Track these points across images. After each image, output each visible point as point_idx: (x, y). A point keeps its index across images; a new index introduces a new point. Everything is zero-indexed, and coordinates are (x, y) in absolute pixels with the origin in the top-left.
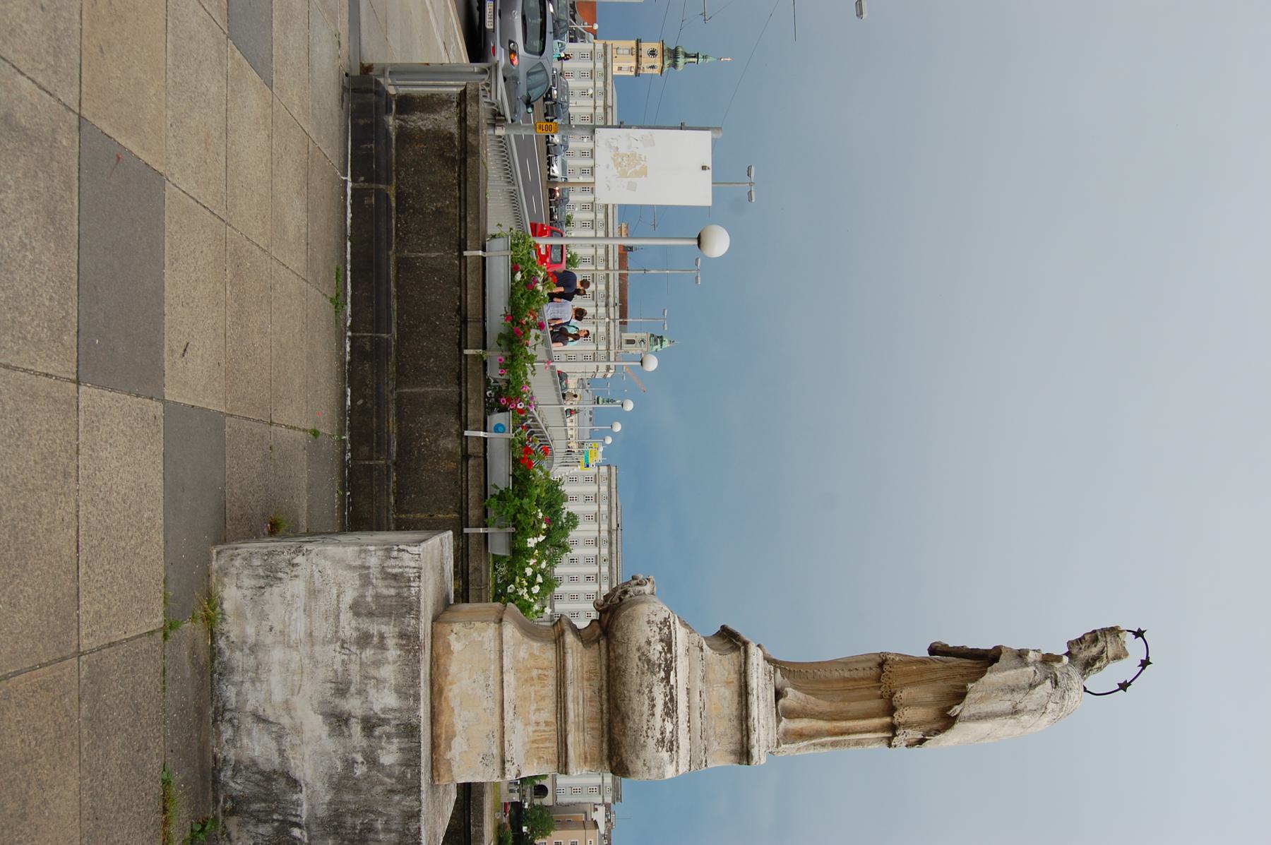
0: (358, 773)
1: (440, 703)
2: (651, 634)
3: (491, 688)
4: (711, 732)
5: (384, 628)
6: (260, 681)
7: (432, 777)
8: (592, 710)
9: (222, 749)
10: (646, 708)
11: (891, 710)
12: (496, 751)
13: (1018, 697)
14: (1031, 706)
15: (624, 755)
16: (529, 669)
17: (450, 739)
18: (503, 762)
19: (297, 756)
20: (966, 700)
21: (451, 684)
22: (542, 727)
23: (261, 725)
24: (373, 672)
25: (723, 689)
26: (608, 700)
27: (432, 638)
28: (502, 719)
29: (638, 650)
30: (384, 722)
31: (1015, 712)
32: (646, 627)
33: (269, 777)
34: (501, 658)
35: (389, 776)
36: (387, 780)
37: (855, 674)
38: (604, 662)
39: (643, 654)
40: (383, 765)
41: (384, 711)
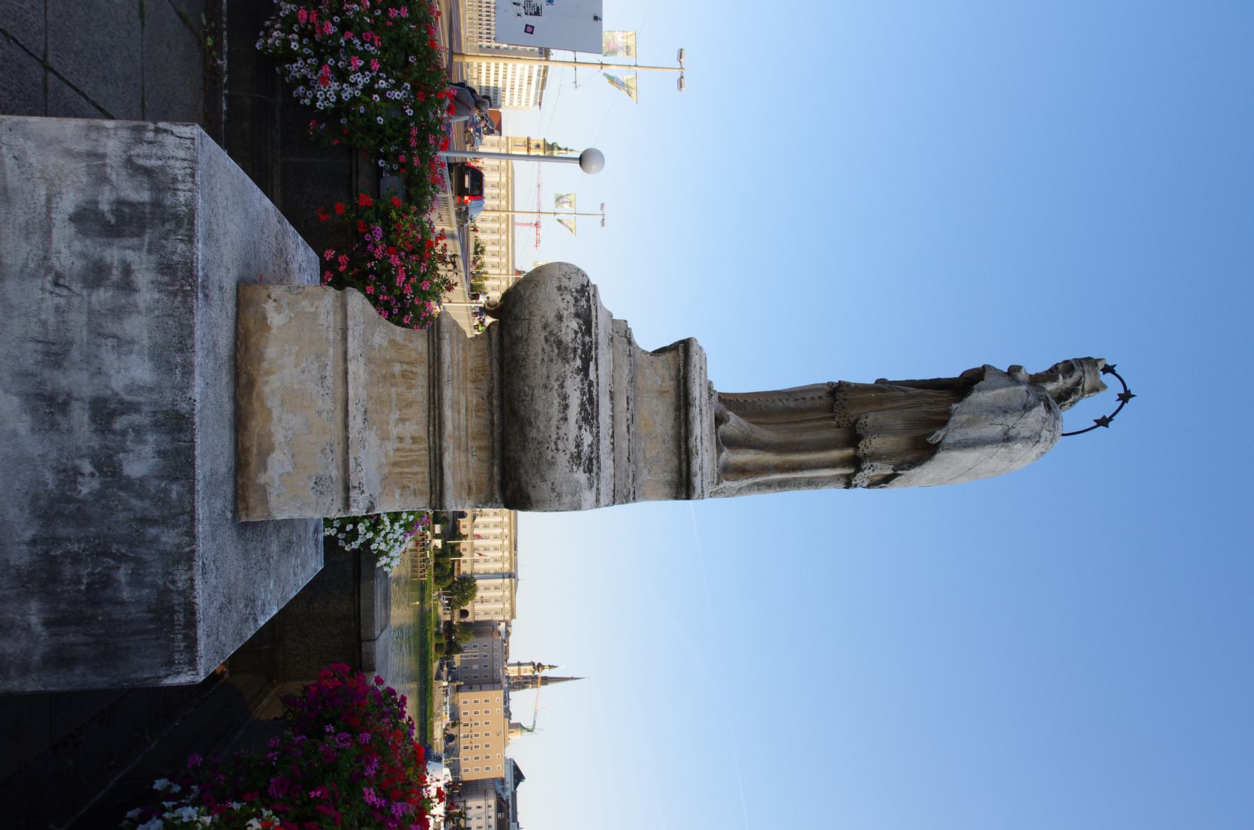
0: (85, 490)
2: (563, 305)
3: (329, 381)
4: (640, 456)
5: (131, 256)
7: (235, 512)
8: (476, 423)
10: (555, 410)
12: (335, 473)
13: (1011, 420)
14: (1026, 433)
15: (524, 478)
16: (389, 363)
18: (347, 489)
20: (951, 424)
21: (268, 373)
22: (408, 444)
24: (111, 327)
25: (655, 401)
26: (502, 407)
27: (238, 305)
28: (346, 426)
29: (545, 327)
30: (132, 408)
32: (555, 294)
34: (345, 339)
35: (141, 497)
36: (136, 503)
38: (495, 354)
39: (551, 333)
40: (128, 478)
41: (130, 389)
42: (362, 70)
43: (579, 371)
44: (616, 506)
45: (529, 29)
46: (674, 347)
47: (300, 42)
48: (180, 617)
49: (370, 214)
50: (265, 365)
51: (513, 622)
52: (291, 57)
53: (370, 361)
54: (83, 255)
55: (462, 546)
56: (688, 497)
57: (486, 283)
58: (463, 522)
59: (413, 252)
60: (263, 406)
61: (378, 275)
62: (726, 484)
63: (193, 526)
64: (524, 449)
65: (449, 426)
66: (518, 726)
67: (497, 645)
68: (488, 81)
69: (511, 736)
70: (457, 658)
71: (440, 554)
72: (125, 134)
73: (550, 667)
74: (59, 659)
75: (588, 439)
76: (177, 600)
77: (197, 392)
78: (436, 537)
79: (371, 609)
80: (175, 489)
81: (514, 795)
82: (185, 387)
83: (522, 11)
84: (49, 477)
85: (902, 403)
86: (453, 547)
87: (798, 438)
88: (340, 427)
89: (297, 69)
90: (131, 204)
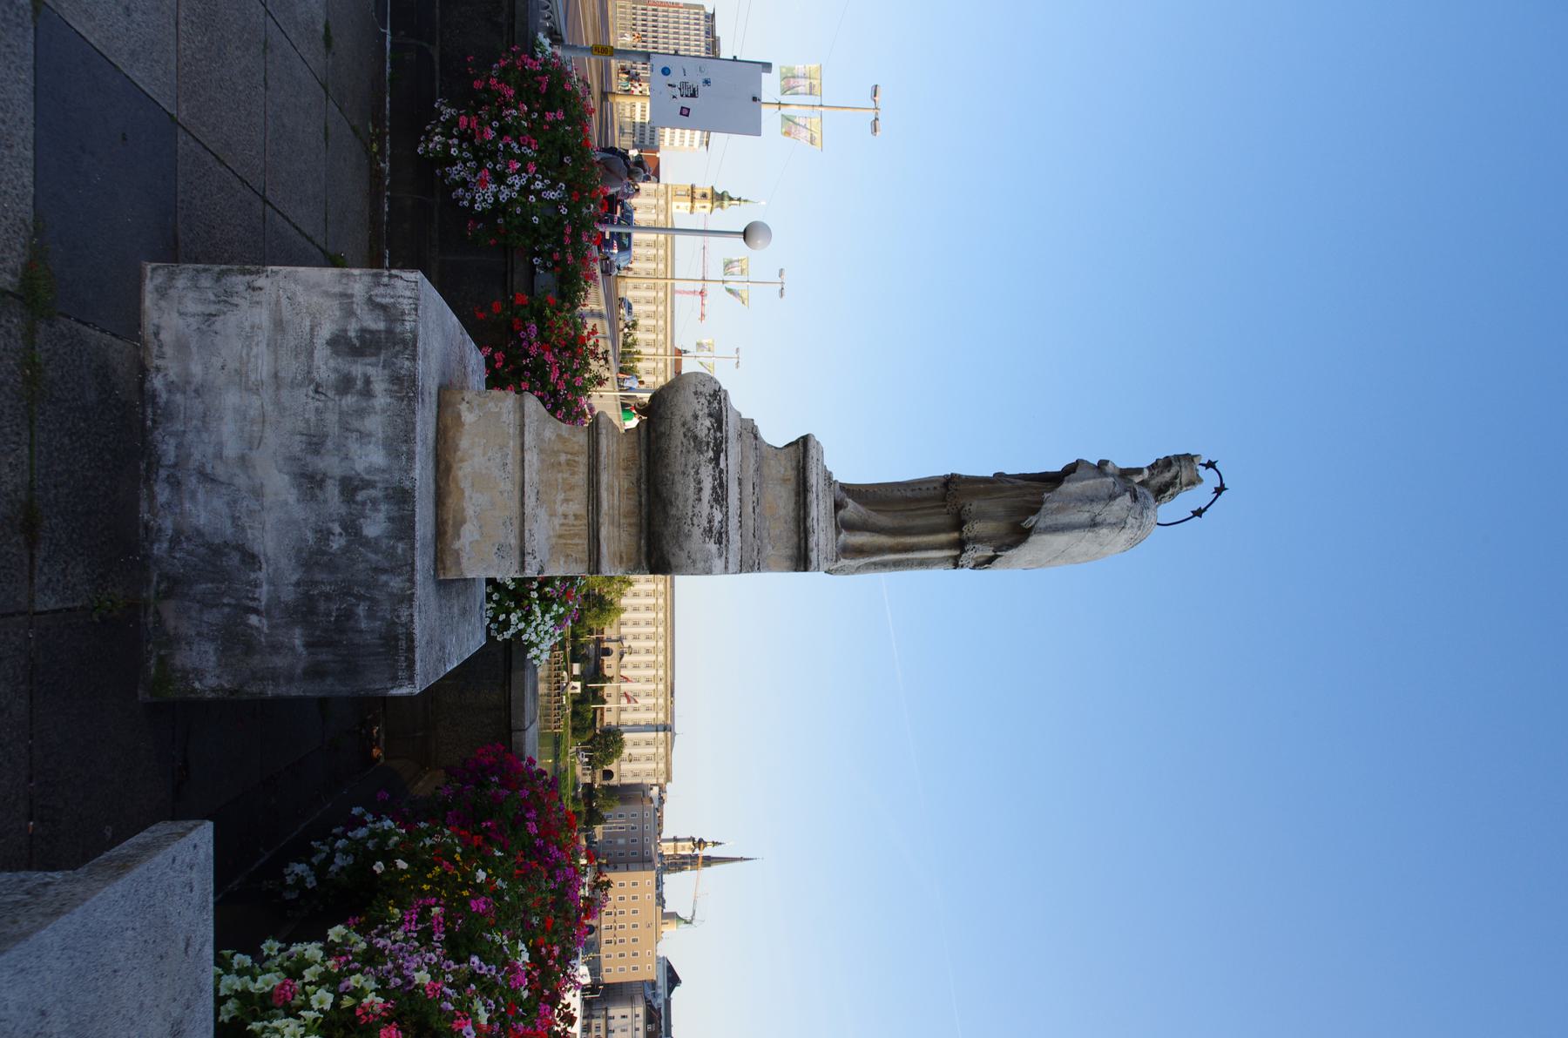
0: (335, 546)
3: (510, 467)
4: (765, 534)
5: (371, 371)
6: (207, 430)
7: (436, 570)
8: (627, 504)
9: (155, 515)
10: (691, 492)
11: (959, 525)
12: (514, 542)
13: (1097, 508)
14: (1113, 520)
17: (459, 523)
18: (523, 554)
19: (256, 525)
21: (462, 461)
22: (571, 520)
23: (209, 486)
24: (356, 424)
27: (439, 406)
28: (523, 504)
30: (369, 484)
31: (1094, 524)
32: (692, 398)
33: (217, 551)
34: (522, 434)
35: (376, 553)
36: (371, 556)
38: (644, 447)
41: (369, 470)
42: (519, 172)
43: (711, 460)
44: (743, 575)
45: (685, 112)
46: (796, 442)
47: (460, 146)
48: (403, 644)
49: (525, 312)
50: (459, 454)
51: (669, 787)
52: (452, 162)
53: (541, 451)
54: (336, 370)
55: (606, 691)
56: (806, 570)
57: (639, 365)
58: (607, 660)
59: (566, 348)
60: (458, 487)
61: (533, 372)
62: (843, 562)
63: (413, 575)
64: (666, 524)
65: (605, 506)
66: (673, 916)
67: (648, 814)
68: (643, 116)
69: (665, 929)
70: (599, 830)
71: (578, 701)
72: (367, 279)
73: (715, 844)
74: (315, 672)
75: (718, 516)
76: (401, 630)
77: (417, 473)
78: (575, 678)
79: (522, 699)
80: (400, 547)
81: (668, 1002)
82: (408, 469)
83: (678, 93)
84: (310, 536)
86: (595, 691)
87: (911, 523)
88: (518, 505)
89: (457, 172)
90: (371, 332)
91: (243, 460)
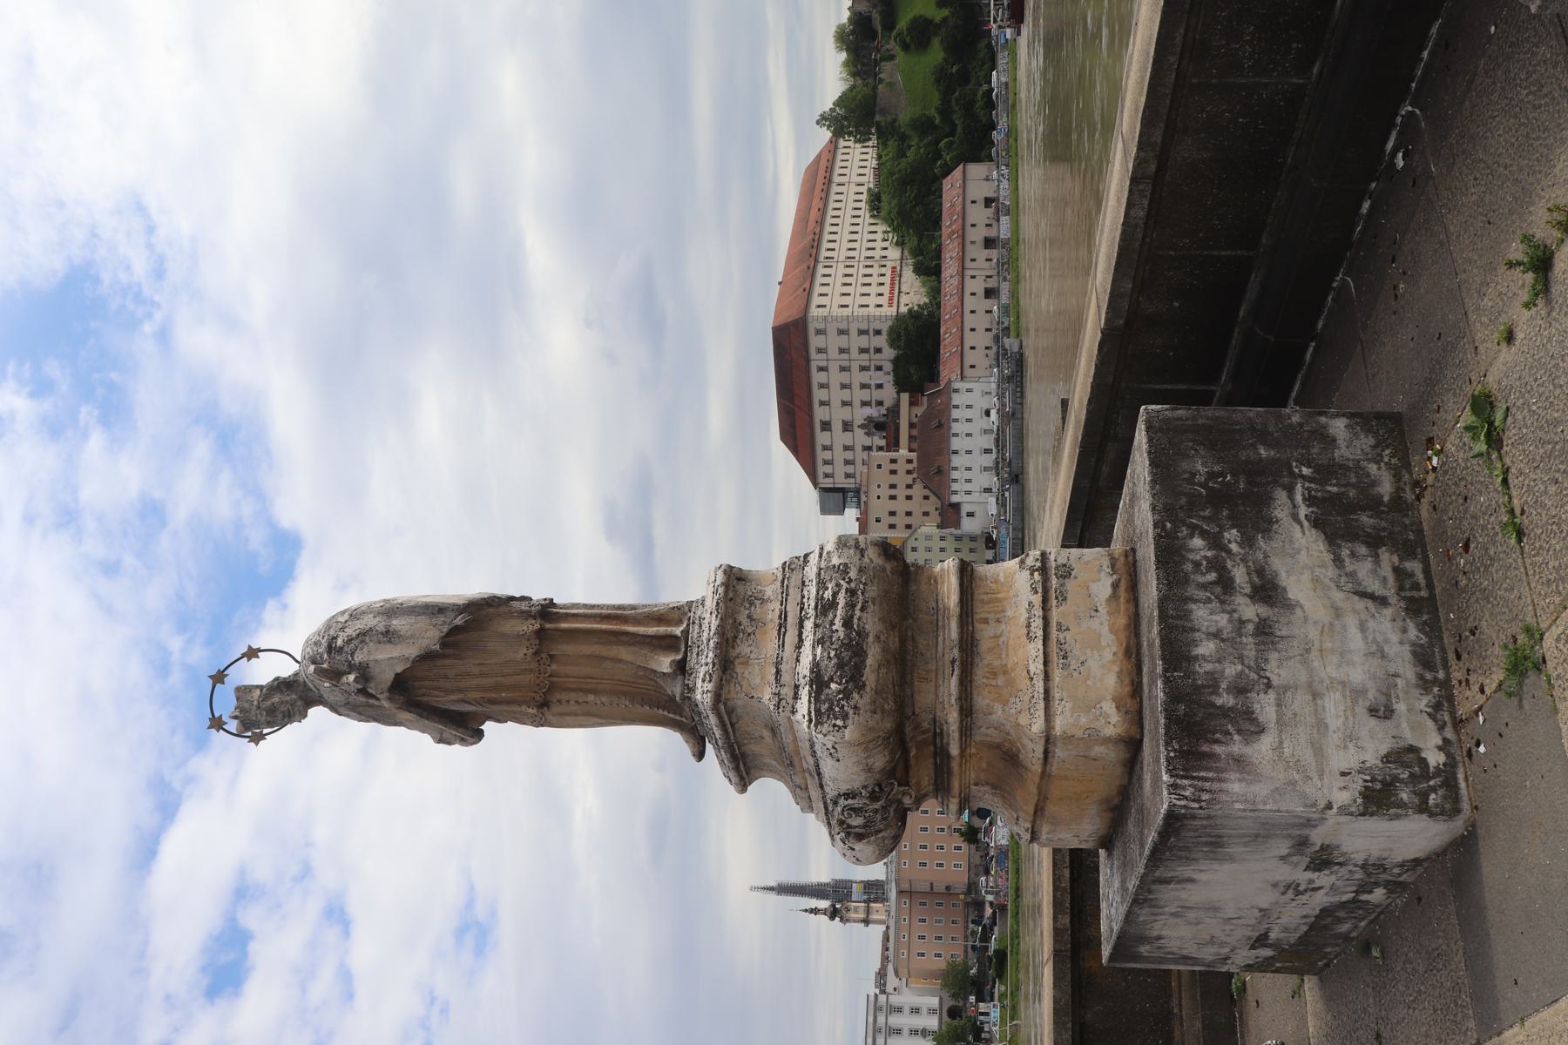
1: (1128, 638)
11: (540, 633)
17: (1115, 595)
21: (1113, 662)
34: (1047, 691)
37: (581, 697)
50: (1117, 669)
73: (815, 911)
85: (475, 682)
91: (1338, 613)
